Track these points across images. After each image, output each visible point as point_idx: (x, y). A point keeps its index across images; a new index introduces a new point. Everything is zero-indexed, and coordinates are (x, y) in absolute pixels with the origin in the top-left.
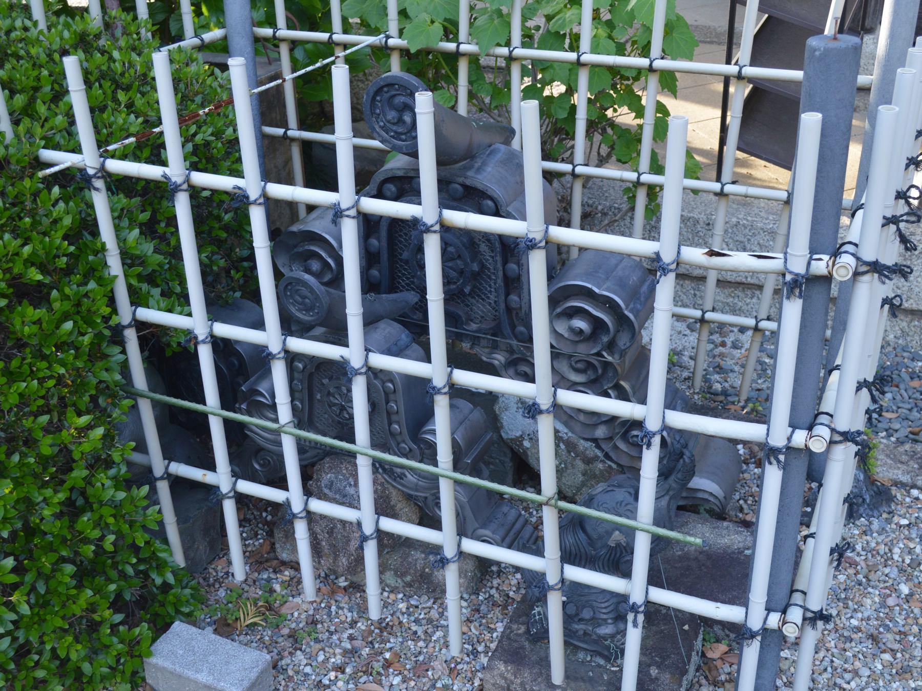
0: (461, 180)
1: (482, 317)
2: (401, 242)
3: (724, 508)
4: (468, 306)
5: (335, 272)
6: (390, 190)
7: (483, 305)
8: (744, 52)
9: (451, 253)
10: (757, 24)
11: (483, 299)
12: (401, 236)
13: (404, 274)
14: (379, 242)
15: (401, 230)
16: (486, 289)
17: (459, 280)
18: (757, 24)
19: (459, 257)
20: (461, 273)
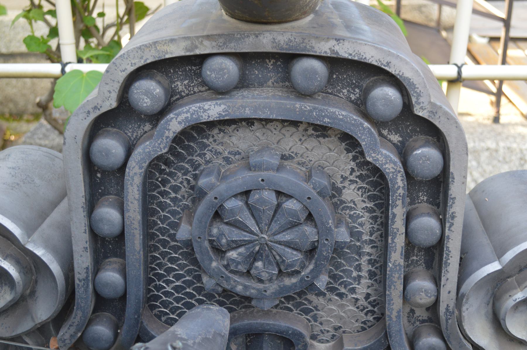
0: (324, 48)
1: (337, 329)
2: (163, 206)
3: (65, 122)
4: (307, 311)
5: (19, 288)
6: (147, 93)
7: (342, 306)
8: (181, 215)
9: (292, 213)
10: (56, 301)
11: (341, 295)
12: (164, 194)
13: (169, 270)
14: (122, 212)
15: (164, 182)
16: (348, 273)
17: (303, 267)
18: (56, 301)
19: (310, 217)
20: (311, 252)
